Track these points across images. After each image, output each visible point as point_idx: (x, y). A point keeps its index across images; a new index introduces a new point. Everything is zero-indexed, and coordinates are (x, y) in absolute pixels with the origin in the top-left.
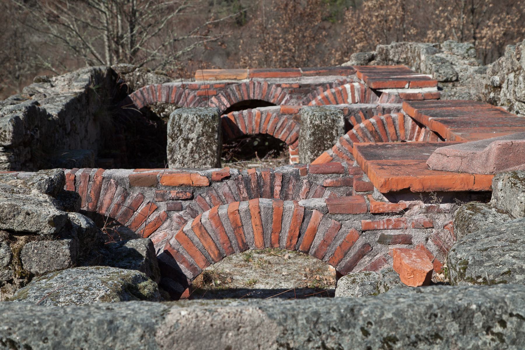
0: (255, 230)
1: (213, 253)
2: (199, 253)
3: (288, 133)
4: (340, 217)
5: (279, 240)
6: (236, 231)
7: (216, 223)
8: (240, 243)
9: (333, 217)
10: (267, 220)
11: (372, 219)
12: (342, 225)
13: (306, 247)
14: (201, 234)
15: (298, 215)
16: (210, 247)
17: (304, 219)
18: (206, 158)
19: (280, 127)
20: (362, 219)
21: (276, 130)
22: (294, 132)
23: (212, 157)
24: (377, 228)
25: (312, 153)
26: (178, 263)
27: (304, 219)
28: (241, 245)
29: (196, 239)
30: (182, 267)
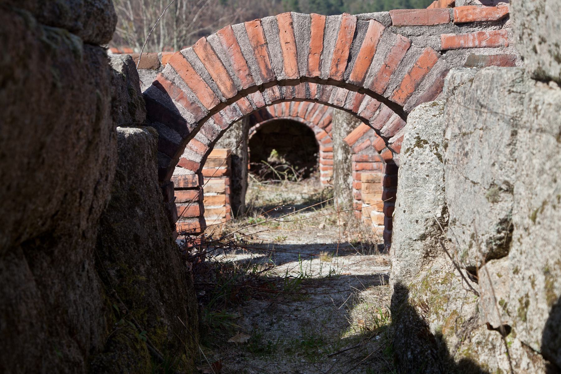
0: (284, 49)
1: (224, 84)
2: (203, 84)
3: (321, 115)
4: (409, 30)
5: (320, 65)
6: (256, 52)
7: (227, 40)
8: (263, 69)
9: (399, 31)
10: (302, 34)
11: (457, 33)
12: (411, 42)
13: (360, 76)
14: (207, 56)
15: (348, 27)
16: (218, 75)
17: (356, 34)
18: (230, 131)
19: (313, 108)
20: (441, 32)
21: (308, 112)
22: (327, 115)
23: (237, 129)
24: (464, 46)
25: (348, 124)
26: (173, 101)
27: (356, 34)
28: (264, 73)
29: (199, 65)
30: (179, 106)
